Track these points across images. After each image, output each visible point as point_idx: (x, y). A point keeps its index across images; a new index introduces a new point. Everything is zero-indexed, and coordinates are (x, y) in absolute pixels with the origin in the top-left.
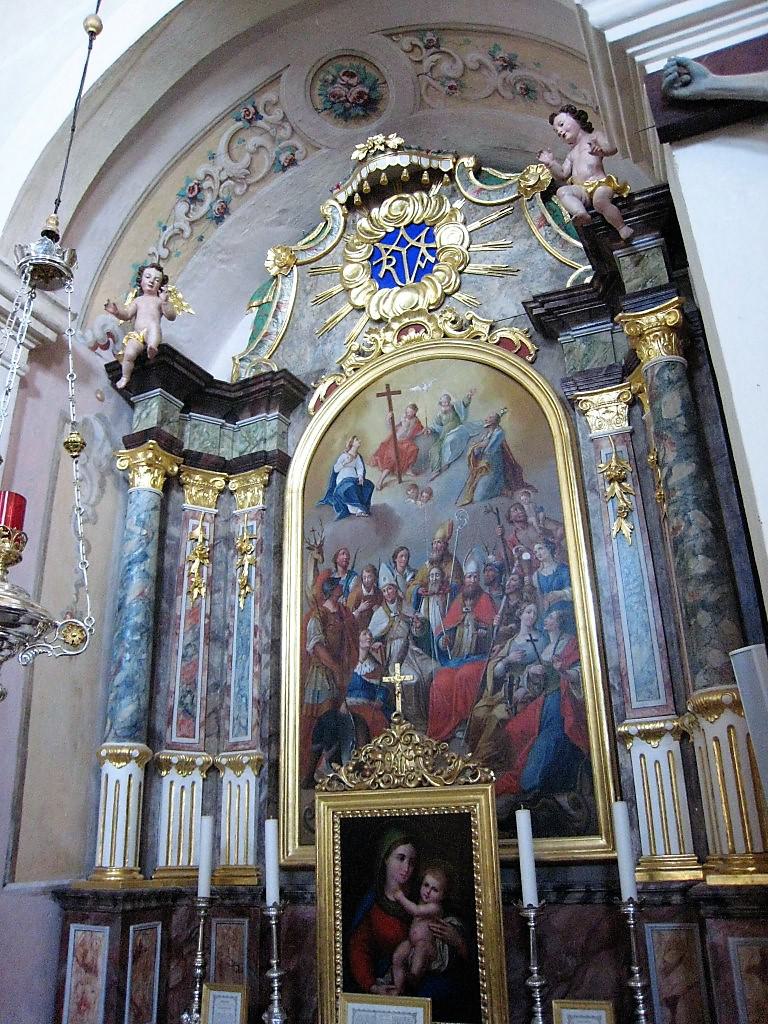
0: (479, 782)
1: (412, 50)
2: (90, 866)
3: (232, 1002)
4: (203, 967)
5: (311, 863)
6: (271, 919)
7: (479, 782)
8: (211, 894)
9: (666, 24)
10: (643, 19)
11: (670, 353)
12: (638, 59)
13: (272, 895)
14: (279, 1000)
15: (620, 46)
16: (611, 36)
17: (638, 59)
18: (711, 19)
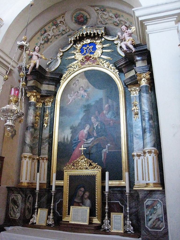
0: (98, 169)
1: (60, 23)
2: (19, 182)
3: (45, 212)
4: (53, 206)
5: (124, 185)
6: (52, 194)
7: (98, 169)
8: (39, 189)
9: (149, 19)
10: (148, 16)
11: (35, 101)
12: (145, 24)
13: (38, 189)
14: (53, 212)
15: (142, 22)
16: (140, 19)
17: (145, 24)
18: (170, 17)
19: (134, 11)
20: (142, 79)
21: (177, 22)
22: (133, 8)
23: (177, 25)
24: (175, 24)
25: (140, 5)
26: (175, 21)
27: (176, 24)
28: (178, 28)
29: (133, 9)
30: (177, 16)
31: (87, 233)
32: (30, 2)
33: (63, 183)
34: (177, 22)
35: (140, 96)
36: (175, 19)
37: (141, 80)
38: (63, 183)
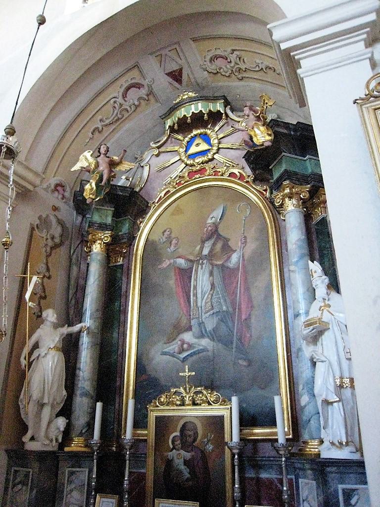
15: (288, 51)
16: (284, 46)
17: (296, 57)
19: (271, 29)
20: (97, 240)
21: (371, 42)
22: (268, 24)
23: (370, 49)
24: (364, 47)
25: (284, 16)
26: (365, 40)
27: (366, 47)
28: (372, 55)
29: (268, 26)
30: (368, 29)
31: (126, 344)
32: (37, 17)
33: (146, 432)
34: (371, 42)
35: (79, 245)
36: (365, 36)
37: (95, 242)
38: (146, 432)
